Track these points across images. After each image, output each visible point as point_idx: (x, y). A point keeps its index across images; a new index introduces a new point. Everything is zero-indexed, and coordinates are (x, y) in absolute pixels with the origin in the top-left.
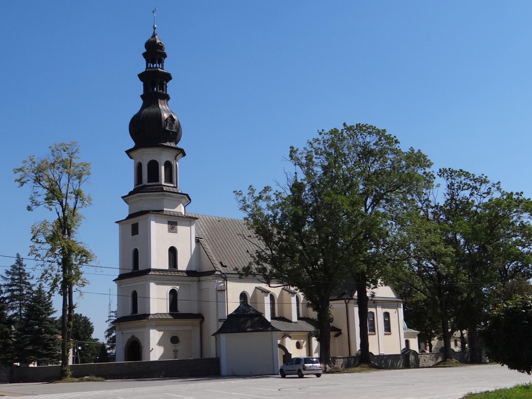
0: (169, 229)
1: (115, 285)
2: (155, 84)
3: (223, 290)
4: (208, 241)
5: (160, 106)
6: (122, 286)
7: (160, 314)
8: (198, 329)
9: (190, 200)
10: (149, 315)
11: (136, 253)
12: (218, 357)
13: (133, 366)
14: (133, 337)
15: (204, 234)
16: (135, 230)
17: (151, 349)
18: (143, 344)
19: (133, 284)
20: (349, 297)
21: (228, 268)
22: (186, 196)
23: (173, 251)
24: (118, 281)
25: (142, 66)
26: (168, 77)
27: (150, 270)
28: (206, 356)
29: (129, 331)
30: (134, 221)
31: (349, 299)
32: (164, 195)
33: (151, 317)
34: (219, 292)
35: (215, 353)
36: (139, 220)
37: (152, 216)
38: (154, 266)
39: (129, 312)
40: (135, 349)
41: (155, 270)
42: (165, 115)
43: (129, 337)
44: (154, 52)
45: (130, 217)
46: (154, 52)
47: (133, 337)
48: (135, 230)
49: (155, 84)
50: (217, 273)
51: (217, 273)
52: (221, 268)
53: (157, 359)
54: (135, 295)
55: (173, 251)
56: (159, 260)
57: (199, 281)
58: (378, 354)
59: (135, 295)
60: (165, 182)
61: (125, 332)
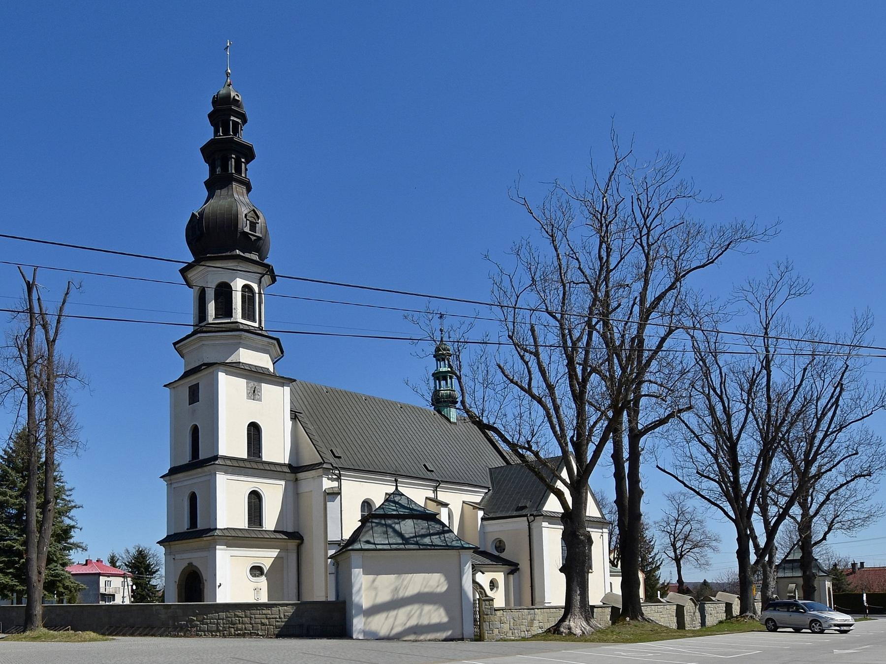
0: (248, 394)
1: (164, 484)
2: (226, 158)
3: (335, 494)
4: (311, 419)
5: (236, 196)
6: (174, 486)
7: (234, 529)
8: (294, 556)
9: (282, 352)
10: (216, 529)
11: (195, 431)
12: (341, 599)
13: (187, 605)
14: (190, 564)
15: (304, 408)
16: (194, 395)
17: (218, 584)
18: (205, 575)
19: (190, 481)
20: (535, 513)
21: (342, 460)
22: (275, 342)
23: (254, 431)
24: (168, 478)
25: (208, 133)
26: (248, 153)
27: (216, 458)
28: (307, 597)
29: (185, 556)
30: (192, 380)
31: (535, 516)
32: (240, 337)
33: (217, 532)
34: (336, 490)
35: (323, 594)
36: (199, 379)
37: (221, 367)
38: (222, 452)
39: (185, 526)
40: (194, 583)
41: (225, 458)
42: (244, 211)
43: (184, 565)
44: (224, 112)
45: (187, 374)
46: (224, 112)
47: (190, 564)
48: (194, 395)
49: (226, 158)
50: (325, 466)
51: (325, 466)
52: (332, 460)
53: (442, 611)
54: (193, 498)
55: (254, 431)
56: (231, 443)
57: (297, 480)
58: (323, 599)
59: (193, 498)
60: (243, 317)
61: (178, 557)
